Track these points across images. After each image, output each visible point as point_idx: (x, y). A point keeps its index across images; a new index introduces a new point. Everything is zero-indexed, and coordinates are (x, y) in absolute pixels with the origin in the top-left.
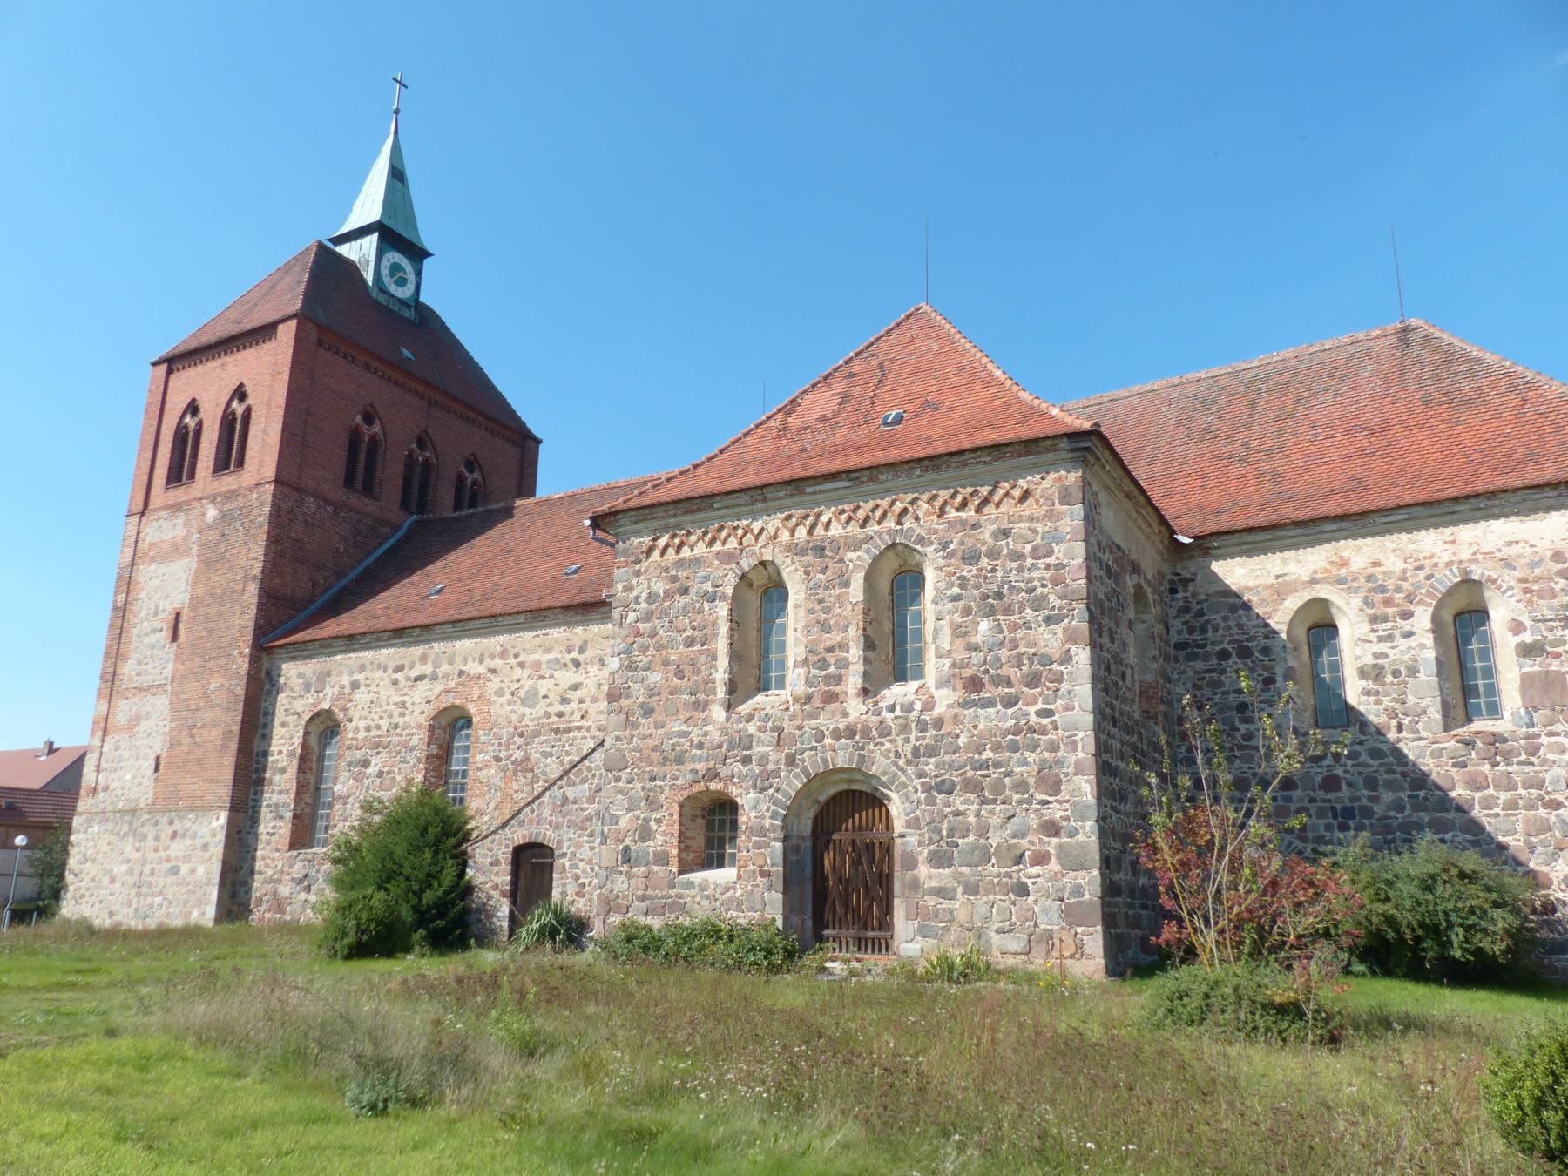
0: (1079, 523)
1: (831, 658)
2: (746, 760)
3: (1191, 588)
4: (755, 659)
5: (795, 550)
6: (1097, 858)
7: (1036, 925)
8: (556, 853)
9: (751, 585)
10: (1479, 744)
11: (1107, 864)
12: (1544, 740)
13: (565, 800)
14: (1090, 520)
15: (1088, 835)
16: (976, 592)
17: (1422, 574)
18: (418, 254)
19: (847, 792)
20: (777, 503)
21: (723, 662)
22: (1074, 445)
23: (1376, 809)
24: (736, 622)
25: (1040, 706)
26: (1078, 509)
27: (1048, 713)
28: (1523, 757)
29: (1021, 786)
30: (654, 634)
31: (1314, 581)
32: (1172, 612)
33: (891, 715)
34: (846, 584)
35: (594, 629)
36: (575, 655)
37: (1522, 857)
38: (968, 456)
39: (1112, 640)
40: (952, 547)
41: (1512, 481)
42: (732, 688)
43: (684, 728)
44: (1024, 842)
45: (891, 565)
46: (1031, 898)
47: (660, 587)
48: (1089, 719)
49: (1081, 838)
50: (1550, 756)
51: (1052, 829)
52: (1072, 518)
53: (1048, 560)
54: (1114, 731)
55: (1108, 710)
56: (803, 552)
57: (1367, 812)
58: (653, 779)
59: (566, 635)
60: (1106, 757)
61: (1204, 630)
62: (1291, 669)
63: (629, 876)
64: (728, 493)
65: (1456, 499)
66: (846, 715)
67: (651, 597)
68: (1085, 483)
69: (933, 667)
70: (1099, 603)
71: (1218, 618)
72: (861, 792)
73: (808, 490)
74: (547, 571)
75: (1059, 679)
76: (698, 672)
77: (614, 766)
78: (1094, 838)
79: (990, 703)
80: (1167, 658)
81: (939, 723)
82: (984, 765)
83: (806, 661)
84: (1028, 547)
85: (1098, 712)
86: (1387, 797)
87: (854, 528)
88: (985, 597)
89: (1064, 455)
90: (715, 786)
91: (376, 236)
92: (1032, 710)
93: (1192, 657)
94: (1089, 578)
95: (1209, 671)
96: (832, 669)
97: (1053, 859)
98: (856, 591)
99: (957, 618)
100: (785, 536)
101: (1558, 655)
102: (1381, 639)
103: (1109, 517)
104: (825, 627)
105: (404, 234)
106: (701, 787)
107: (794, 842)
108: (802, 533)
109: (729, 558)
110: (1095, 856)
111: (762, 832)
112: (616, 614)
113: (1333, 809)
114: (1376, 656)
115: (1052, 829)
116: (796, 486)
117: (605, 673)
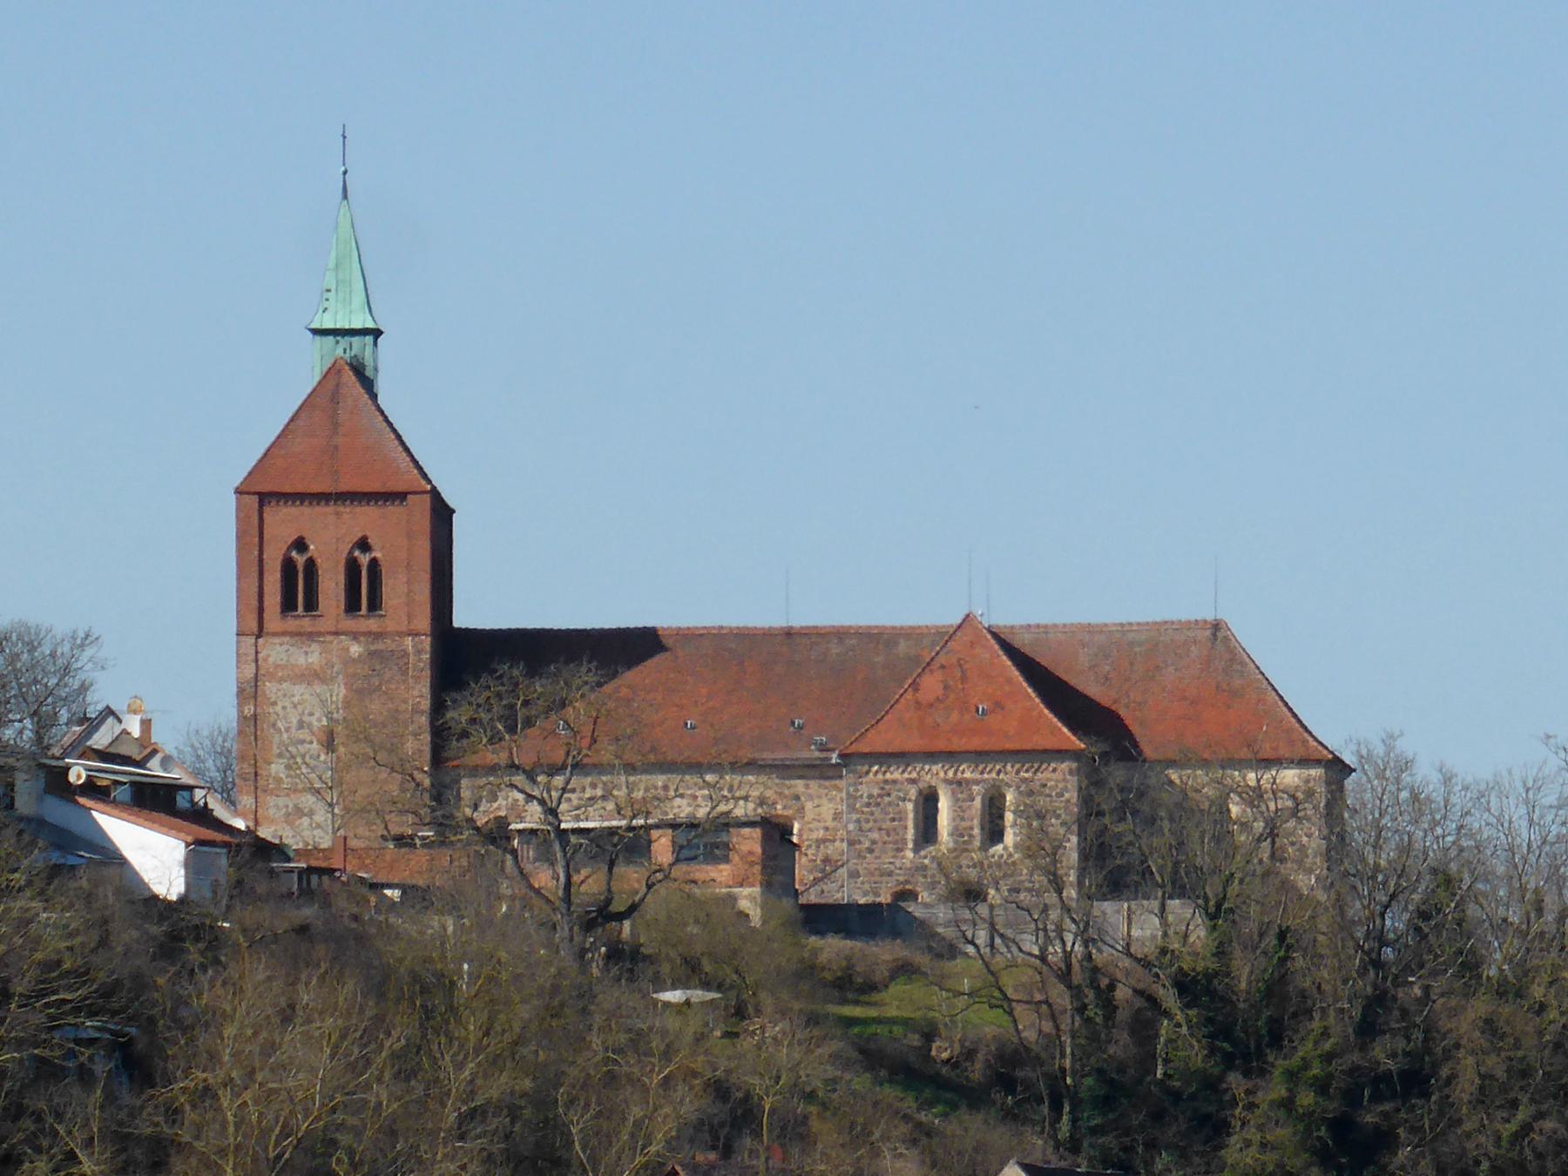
2: (925, 877)
14: (1080, 782)
30: (872, 814)
43: (892, 860)
52: (1073, 781)
67: (870, 796)
76: (898, 834)
90: (907, 887)
98: (978, 802)
104: (963, 819)
108: (951, 774)
109: (913, 781)
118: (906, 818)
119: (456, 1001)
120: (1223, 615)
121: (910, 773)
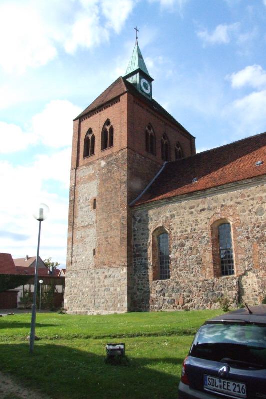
18: (150, 80)
91: (138, 74)
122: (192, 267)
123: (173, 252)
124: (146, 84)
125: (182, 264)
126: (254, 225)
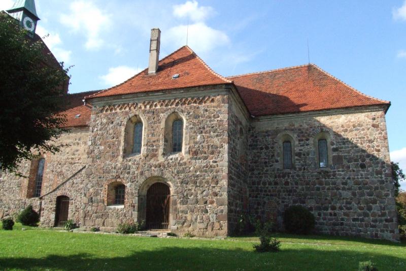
0: (227, 109)
1: (154, 144)
2: (128, 173)
3: (254, 130)
4: (132, 144)
5: (144, 112)
6: (227, 202)
7: (210, 221)
8: (70, 199)
9: (132, 122)
10: (323, 174)
11: (230, 204)
12: (337, 173)
13: (73, 183)
14: (230, 108)
15: (225, 195)
16: (198, 127)
17: (312, 129)
18: (36, 19)
19: (157, 183)
20: (141, 98)
21: (122, 143)
22: (226, 87)
23: (297, 190)
24: (126, 131)
25: (214, 160)
26: (227, 105)
27: (216, 162)
28: (332, 177)
29: (207, 182)
31: (286, 129)
32: (249, 136)
33: (171, 161)
34: (160, 123)
35: (83, 134)
36: (77, 141)
37: (227, 178)
38: (197, 88)
39: (234, 143)
40: (191, 113)
41: (333, 106)
42: (125, 151)
44: (207, 198)
45: (173, 118)
46: (208, 214)
47: (105, 121)
48: (227, 164)
49: (223, 197)
50: (338, 177)
51: (216, 194)
52: (225, 108)
53: (218, 119)
54: (233, 168)
55: (232, 162)
56: (148, 113)
57: (295, 191)
58: (100, 178)
59: (75, 135)
60: (231, 174)
61: (257, 142)
62: (278, 153)
63: (92, 206)
64: (127, 94)
65: (321, 110)
66: (158, 161)
68: (229, 98)
69: (184, 148)
70: (231, 132)
71: (260, 138)
72: (161, 183)
73: (150, 95)
74: (70, 116)
75: (219, 152)
77: (88, 176)
78: (226, 197)
79: (199, 159)
80: (247, 149)
81: (185, 164)
82: (197, 176)
83: (147, 144)
84: (213, 115)
85: (229, 162)
86: (300, 187)
87: (164, 107)
88: (200, 128)
89: (223, 90)
90: (119, 180)
91: (22, 12)
92: (211, 161)
93: (254, 149)
94: (228, 124)
95: (258, 153)
96: (155, 147)
97: (215, 203)
98: (163, 125)
99: (192, 134)
100: (143, 108)
101: (341, 151)
102: (301, 146)
103: (234, 109)
105: (31, 11)
106: (113, 181)
107: (141, 197)
109: (127, 113)
110: (226, 202)
111: (132, 194)
112: (91, 128)
113: (287, 190)
114: (300, 150)
115: (216, 194)
116: (147, 93)
117: (87, 146)
118: (120, 135)
119: (96, 103)
120: (312, 63)
121: (125, 109)
122: (14, 189)
123: (3, 176)
124: (30, 23)
125: (7, 186)
126: (59, 162)
